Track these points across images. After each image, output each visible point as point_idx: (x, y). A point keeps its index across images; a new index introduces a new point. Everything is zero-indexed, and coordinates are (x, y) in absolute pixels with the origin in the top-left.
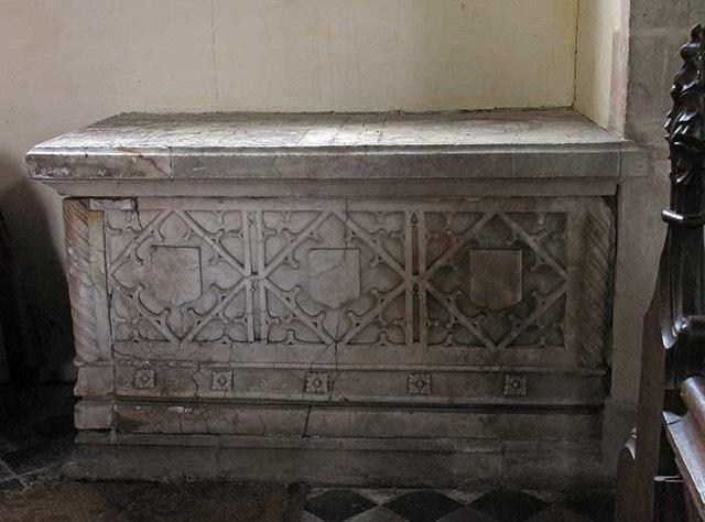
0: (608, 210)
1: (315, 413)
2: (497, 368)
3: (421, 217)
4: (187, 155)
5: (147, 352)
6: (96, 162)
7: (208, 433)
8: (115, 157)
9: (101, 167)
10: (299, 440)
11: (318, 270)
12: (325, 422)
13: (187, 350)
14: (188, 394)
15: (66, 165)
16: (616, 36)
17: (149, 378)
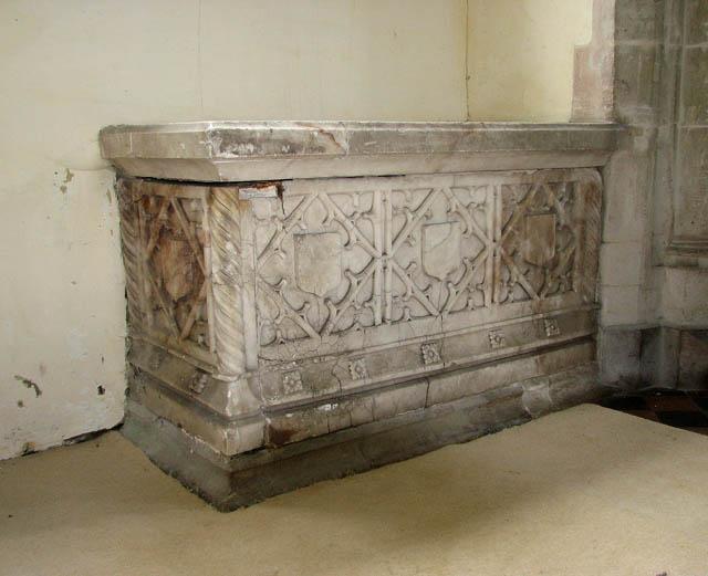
0: (597, 173)
1: (434, 383)
2: (541, 316)
3: (499, 188)
4: (360, 129)
5: (292, 351)
6: (280, 137)
7: (352, 426)
8: (298, 132)
9: (285, 142)
10: (422, 411)
11: (433, 244)
12: (440, 390)
13: (327, 344)
14: (333, 390)
15: (252, 141)
16: (580, 55)
17: (295, 382)
